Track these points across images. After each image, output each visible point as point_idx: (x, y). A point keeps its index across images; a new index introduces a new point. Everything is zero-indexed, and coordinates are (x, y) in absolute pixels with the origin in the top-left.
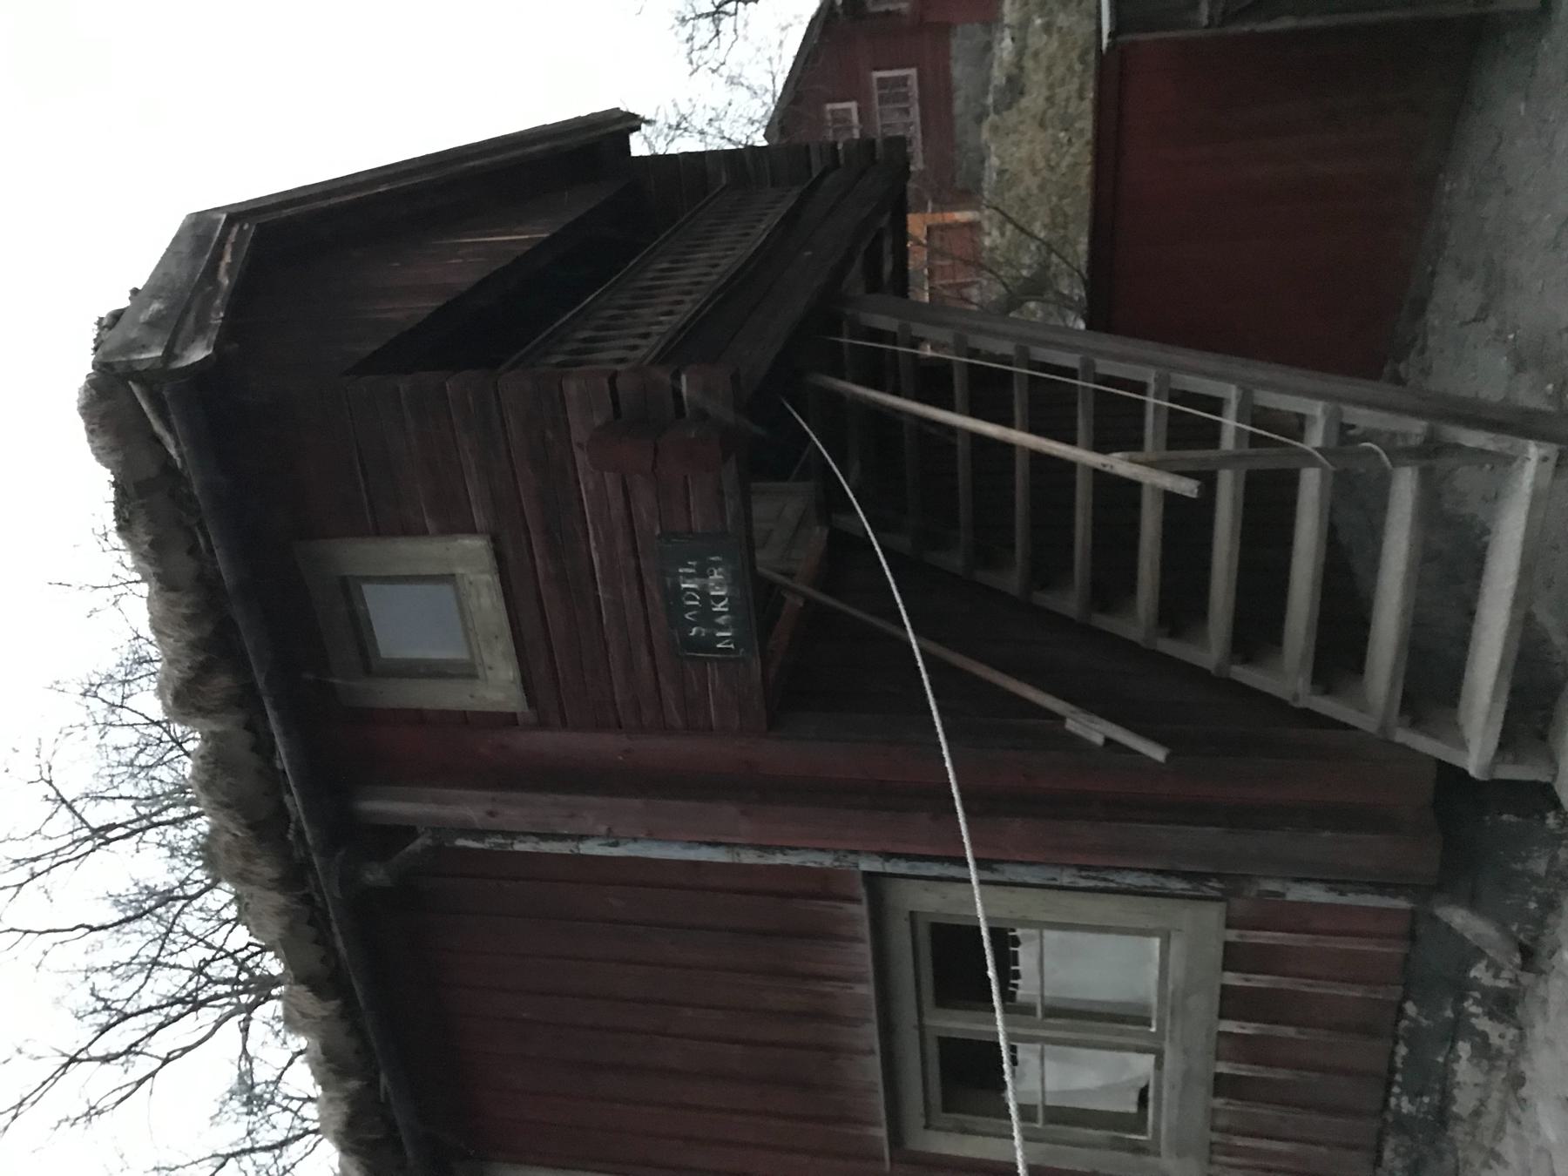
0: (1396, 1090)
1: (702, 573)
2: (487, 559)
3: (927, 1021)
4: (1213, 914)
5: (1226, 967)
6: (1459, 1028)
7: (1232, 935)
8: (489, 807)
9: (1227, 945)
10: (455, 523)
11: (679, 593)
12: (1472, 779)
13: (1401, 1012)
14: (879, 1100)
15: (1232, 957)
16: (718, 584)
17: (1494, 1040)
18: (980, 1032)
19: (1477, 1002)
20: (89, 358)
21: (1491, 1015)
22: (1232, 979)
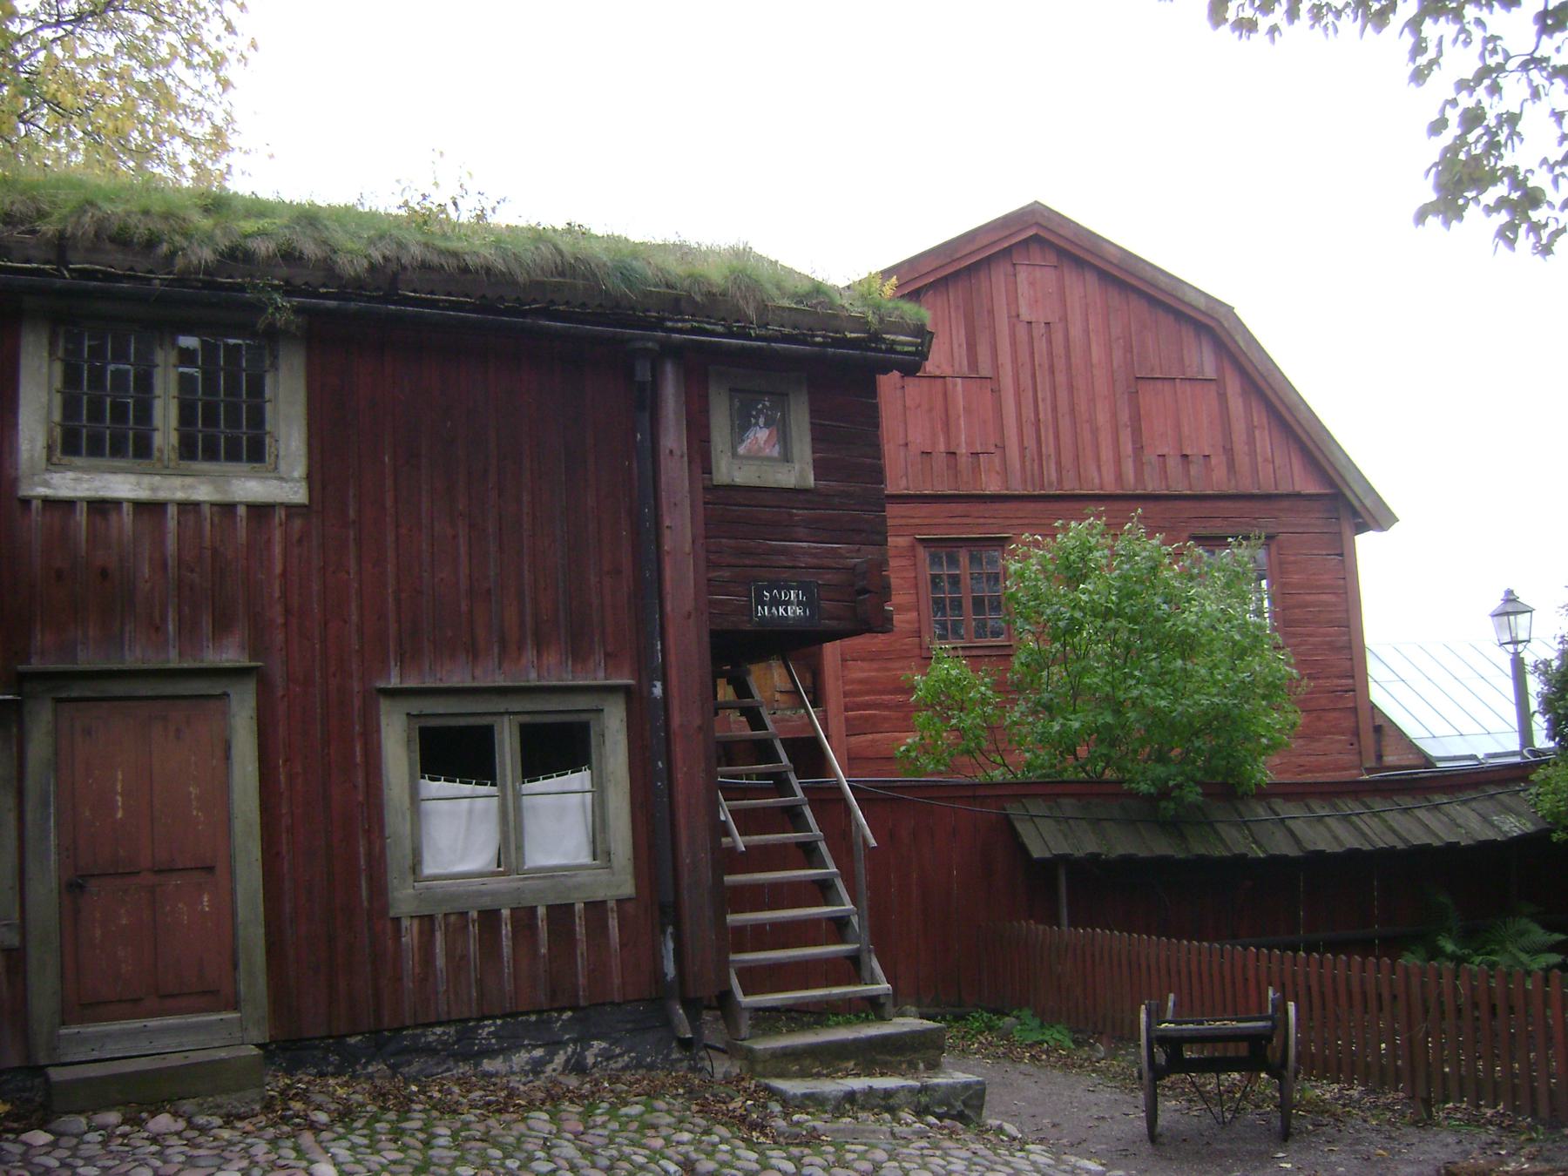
0: (499, 1022)
1: (799, 603)
2: (802, 485)
3: (506, 719)
4: (627, 889)
5: (549, 907)
6: (553, 1045)
7: (612, 904)
8: (677, 453)
9: (604, 902)
10: (820, 468)
11: (789, 588)
12: (1293, 859)
13: (562, 1010)
14: (430, 683)
15: (596, 908)
16: (794, 611)
17: (549, 1068)
18: (502, 756)
19: (574, 1052)
20: (833, 221)
21: (568, 1061)
22: (541, 911)
